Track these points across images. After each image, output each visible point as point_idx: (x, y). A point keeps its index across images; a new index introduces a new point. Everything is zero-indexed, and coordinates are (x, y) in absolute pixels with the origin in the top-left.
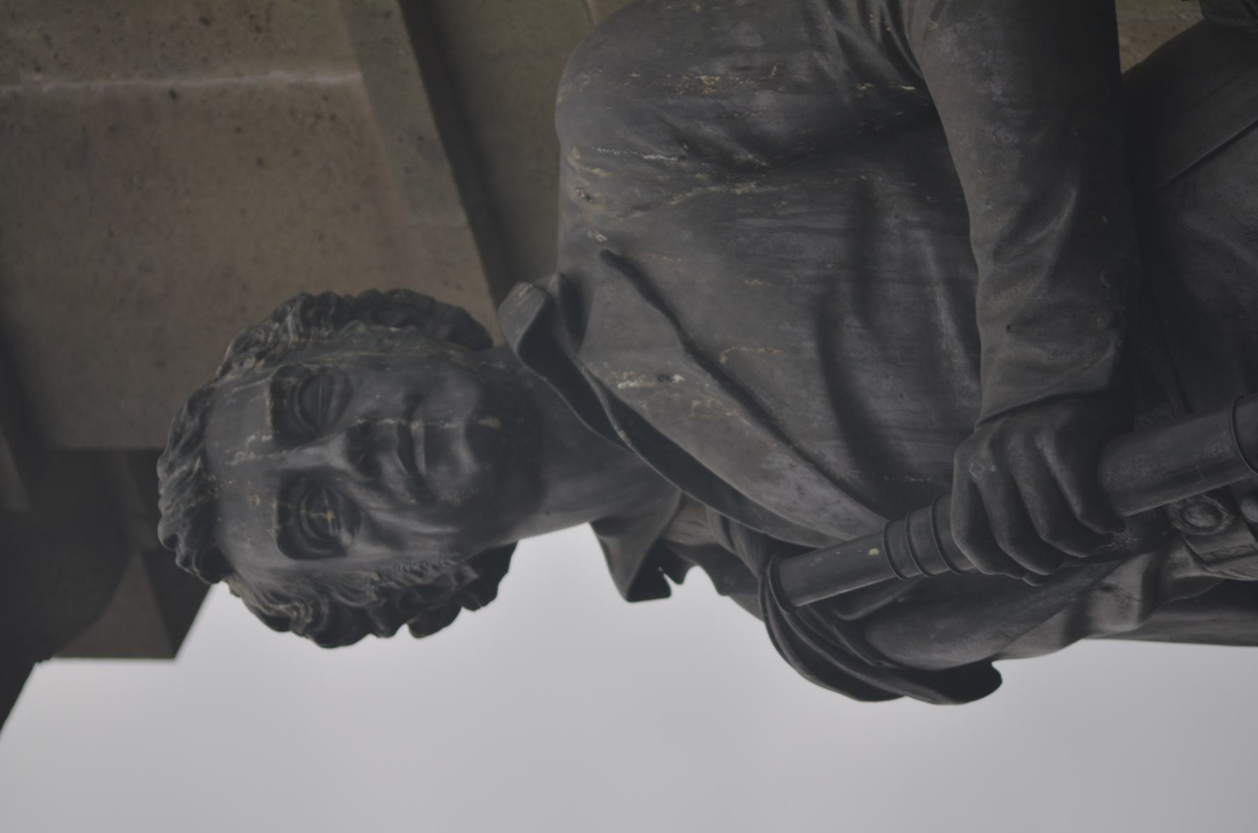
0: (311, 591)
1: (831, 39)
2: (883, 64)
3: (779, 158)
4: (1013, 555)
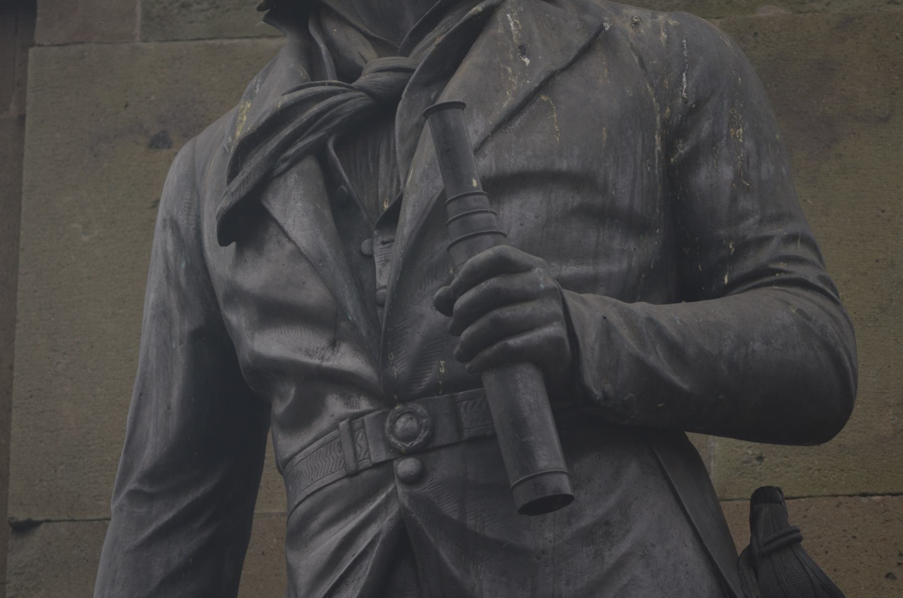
1: (767, 231)
2: (749, 264)
3: (676, 177)
4: (484, 286)
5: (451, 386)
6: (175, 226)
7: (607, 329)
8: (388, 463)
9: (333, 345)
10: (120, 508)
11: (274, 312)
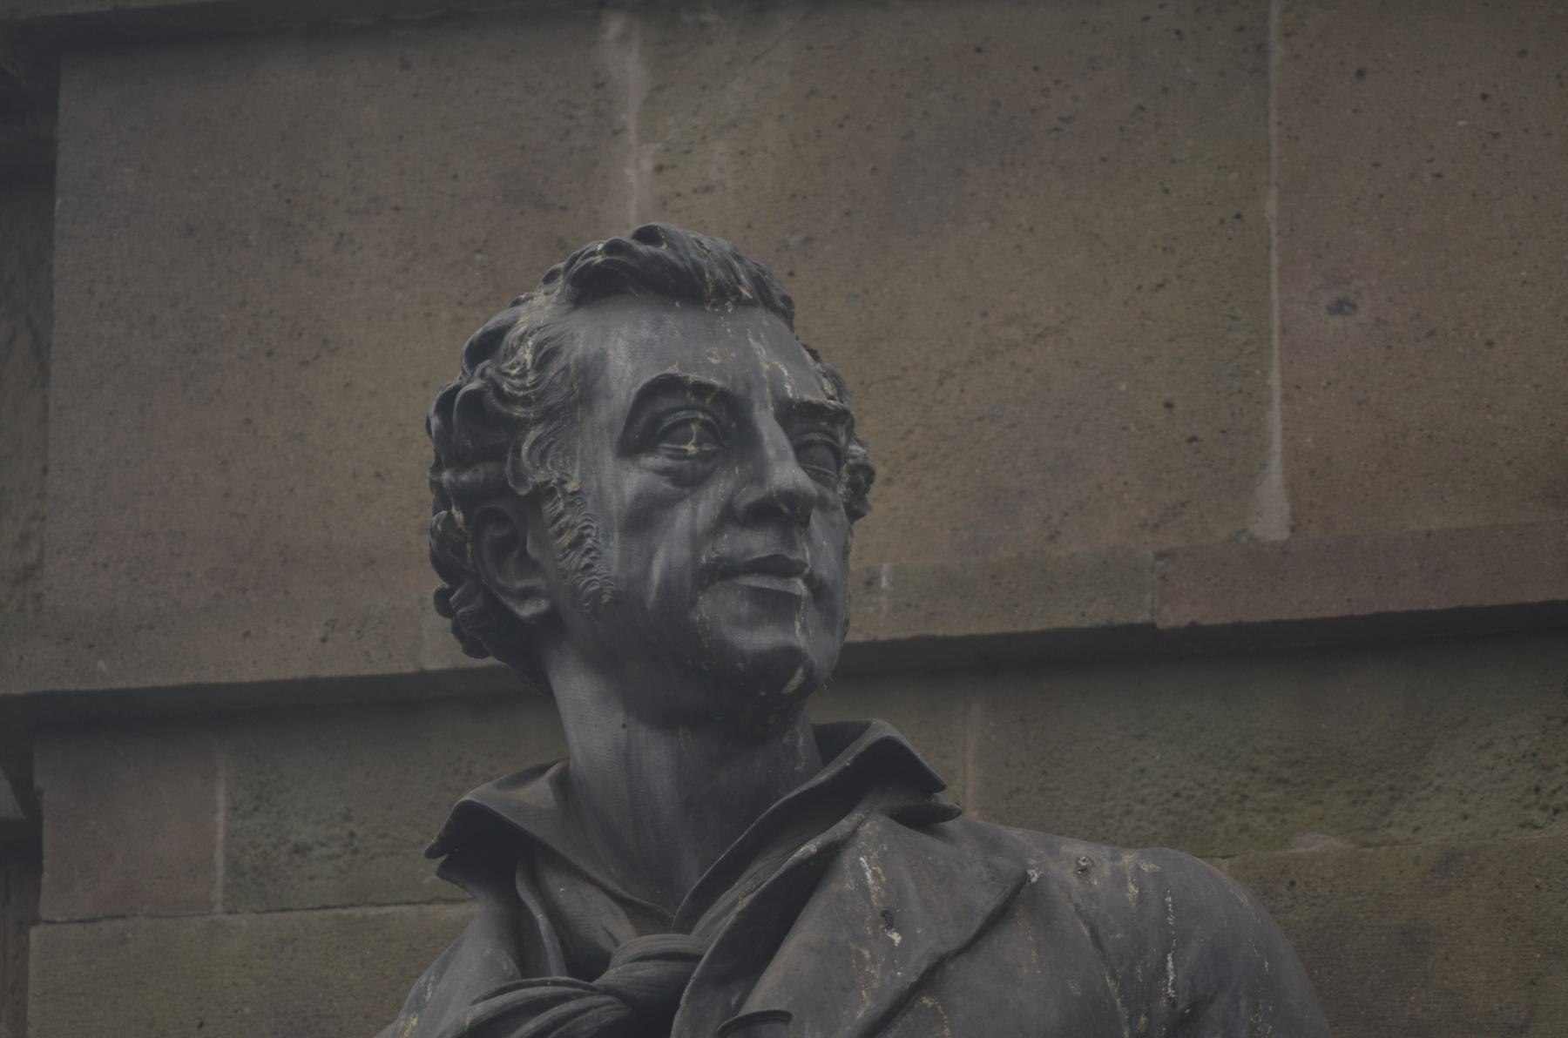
0: (553, 400)
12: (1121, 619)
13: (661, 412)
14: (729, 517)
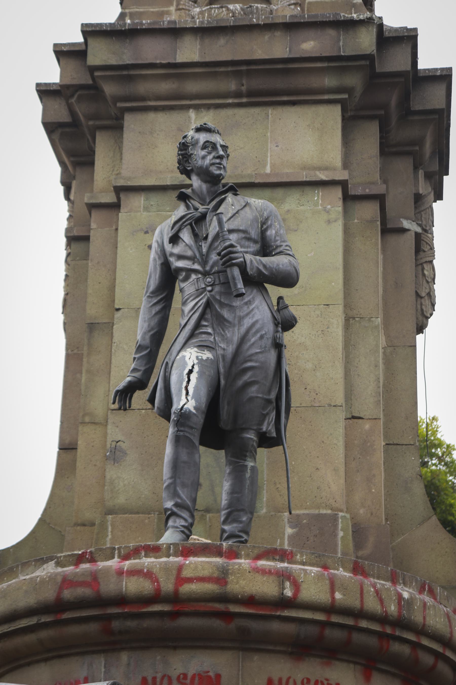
0: (193, 143)
1: (282, 244)
2: (278, 250)
3: (263, 233)
4: (228, 250)
5: (218, 272)
6: (157, 242)
7: (251, 261)
8: (205, 288)
9: (193, 264)
10: (145, 299)
11: (180, 257)
12: (250, 181)
13: (206, 145)
14: (214, 158)
